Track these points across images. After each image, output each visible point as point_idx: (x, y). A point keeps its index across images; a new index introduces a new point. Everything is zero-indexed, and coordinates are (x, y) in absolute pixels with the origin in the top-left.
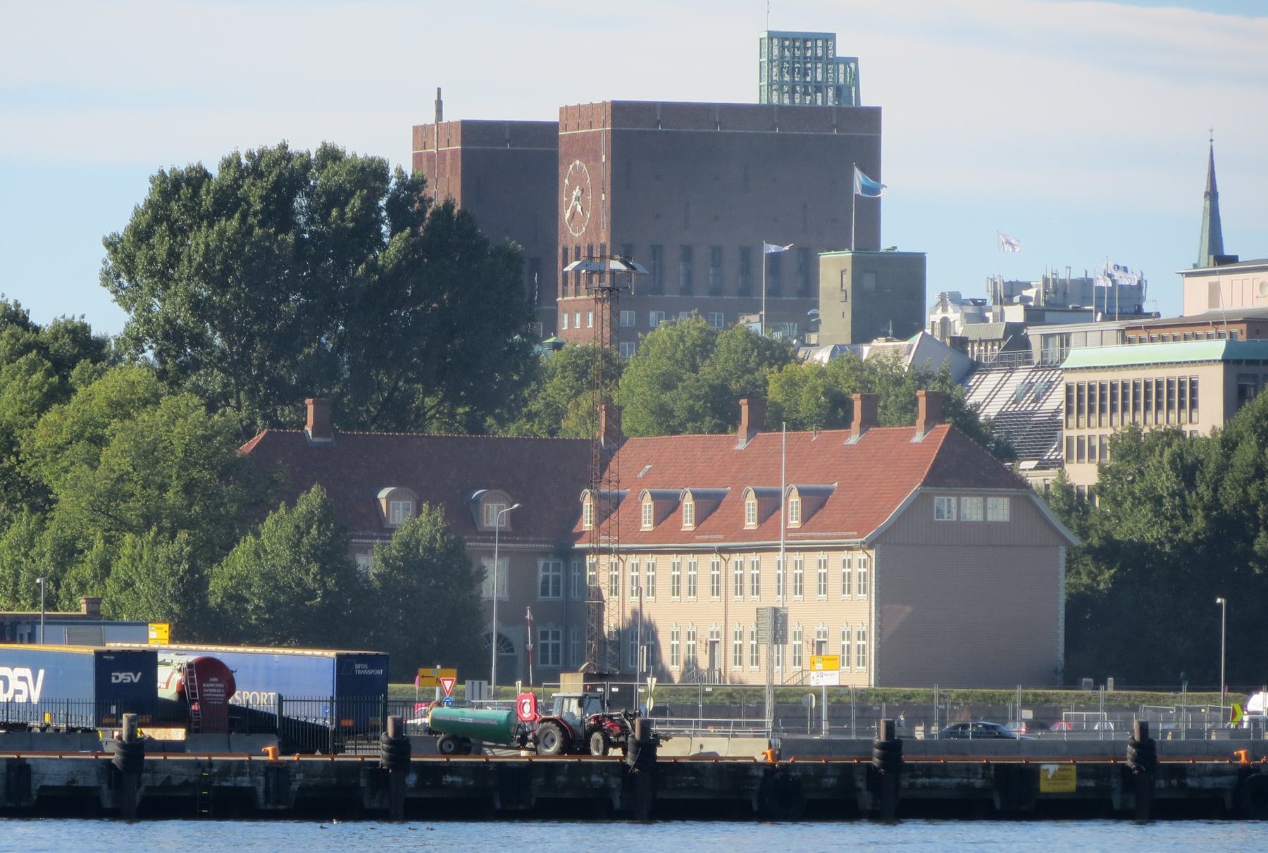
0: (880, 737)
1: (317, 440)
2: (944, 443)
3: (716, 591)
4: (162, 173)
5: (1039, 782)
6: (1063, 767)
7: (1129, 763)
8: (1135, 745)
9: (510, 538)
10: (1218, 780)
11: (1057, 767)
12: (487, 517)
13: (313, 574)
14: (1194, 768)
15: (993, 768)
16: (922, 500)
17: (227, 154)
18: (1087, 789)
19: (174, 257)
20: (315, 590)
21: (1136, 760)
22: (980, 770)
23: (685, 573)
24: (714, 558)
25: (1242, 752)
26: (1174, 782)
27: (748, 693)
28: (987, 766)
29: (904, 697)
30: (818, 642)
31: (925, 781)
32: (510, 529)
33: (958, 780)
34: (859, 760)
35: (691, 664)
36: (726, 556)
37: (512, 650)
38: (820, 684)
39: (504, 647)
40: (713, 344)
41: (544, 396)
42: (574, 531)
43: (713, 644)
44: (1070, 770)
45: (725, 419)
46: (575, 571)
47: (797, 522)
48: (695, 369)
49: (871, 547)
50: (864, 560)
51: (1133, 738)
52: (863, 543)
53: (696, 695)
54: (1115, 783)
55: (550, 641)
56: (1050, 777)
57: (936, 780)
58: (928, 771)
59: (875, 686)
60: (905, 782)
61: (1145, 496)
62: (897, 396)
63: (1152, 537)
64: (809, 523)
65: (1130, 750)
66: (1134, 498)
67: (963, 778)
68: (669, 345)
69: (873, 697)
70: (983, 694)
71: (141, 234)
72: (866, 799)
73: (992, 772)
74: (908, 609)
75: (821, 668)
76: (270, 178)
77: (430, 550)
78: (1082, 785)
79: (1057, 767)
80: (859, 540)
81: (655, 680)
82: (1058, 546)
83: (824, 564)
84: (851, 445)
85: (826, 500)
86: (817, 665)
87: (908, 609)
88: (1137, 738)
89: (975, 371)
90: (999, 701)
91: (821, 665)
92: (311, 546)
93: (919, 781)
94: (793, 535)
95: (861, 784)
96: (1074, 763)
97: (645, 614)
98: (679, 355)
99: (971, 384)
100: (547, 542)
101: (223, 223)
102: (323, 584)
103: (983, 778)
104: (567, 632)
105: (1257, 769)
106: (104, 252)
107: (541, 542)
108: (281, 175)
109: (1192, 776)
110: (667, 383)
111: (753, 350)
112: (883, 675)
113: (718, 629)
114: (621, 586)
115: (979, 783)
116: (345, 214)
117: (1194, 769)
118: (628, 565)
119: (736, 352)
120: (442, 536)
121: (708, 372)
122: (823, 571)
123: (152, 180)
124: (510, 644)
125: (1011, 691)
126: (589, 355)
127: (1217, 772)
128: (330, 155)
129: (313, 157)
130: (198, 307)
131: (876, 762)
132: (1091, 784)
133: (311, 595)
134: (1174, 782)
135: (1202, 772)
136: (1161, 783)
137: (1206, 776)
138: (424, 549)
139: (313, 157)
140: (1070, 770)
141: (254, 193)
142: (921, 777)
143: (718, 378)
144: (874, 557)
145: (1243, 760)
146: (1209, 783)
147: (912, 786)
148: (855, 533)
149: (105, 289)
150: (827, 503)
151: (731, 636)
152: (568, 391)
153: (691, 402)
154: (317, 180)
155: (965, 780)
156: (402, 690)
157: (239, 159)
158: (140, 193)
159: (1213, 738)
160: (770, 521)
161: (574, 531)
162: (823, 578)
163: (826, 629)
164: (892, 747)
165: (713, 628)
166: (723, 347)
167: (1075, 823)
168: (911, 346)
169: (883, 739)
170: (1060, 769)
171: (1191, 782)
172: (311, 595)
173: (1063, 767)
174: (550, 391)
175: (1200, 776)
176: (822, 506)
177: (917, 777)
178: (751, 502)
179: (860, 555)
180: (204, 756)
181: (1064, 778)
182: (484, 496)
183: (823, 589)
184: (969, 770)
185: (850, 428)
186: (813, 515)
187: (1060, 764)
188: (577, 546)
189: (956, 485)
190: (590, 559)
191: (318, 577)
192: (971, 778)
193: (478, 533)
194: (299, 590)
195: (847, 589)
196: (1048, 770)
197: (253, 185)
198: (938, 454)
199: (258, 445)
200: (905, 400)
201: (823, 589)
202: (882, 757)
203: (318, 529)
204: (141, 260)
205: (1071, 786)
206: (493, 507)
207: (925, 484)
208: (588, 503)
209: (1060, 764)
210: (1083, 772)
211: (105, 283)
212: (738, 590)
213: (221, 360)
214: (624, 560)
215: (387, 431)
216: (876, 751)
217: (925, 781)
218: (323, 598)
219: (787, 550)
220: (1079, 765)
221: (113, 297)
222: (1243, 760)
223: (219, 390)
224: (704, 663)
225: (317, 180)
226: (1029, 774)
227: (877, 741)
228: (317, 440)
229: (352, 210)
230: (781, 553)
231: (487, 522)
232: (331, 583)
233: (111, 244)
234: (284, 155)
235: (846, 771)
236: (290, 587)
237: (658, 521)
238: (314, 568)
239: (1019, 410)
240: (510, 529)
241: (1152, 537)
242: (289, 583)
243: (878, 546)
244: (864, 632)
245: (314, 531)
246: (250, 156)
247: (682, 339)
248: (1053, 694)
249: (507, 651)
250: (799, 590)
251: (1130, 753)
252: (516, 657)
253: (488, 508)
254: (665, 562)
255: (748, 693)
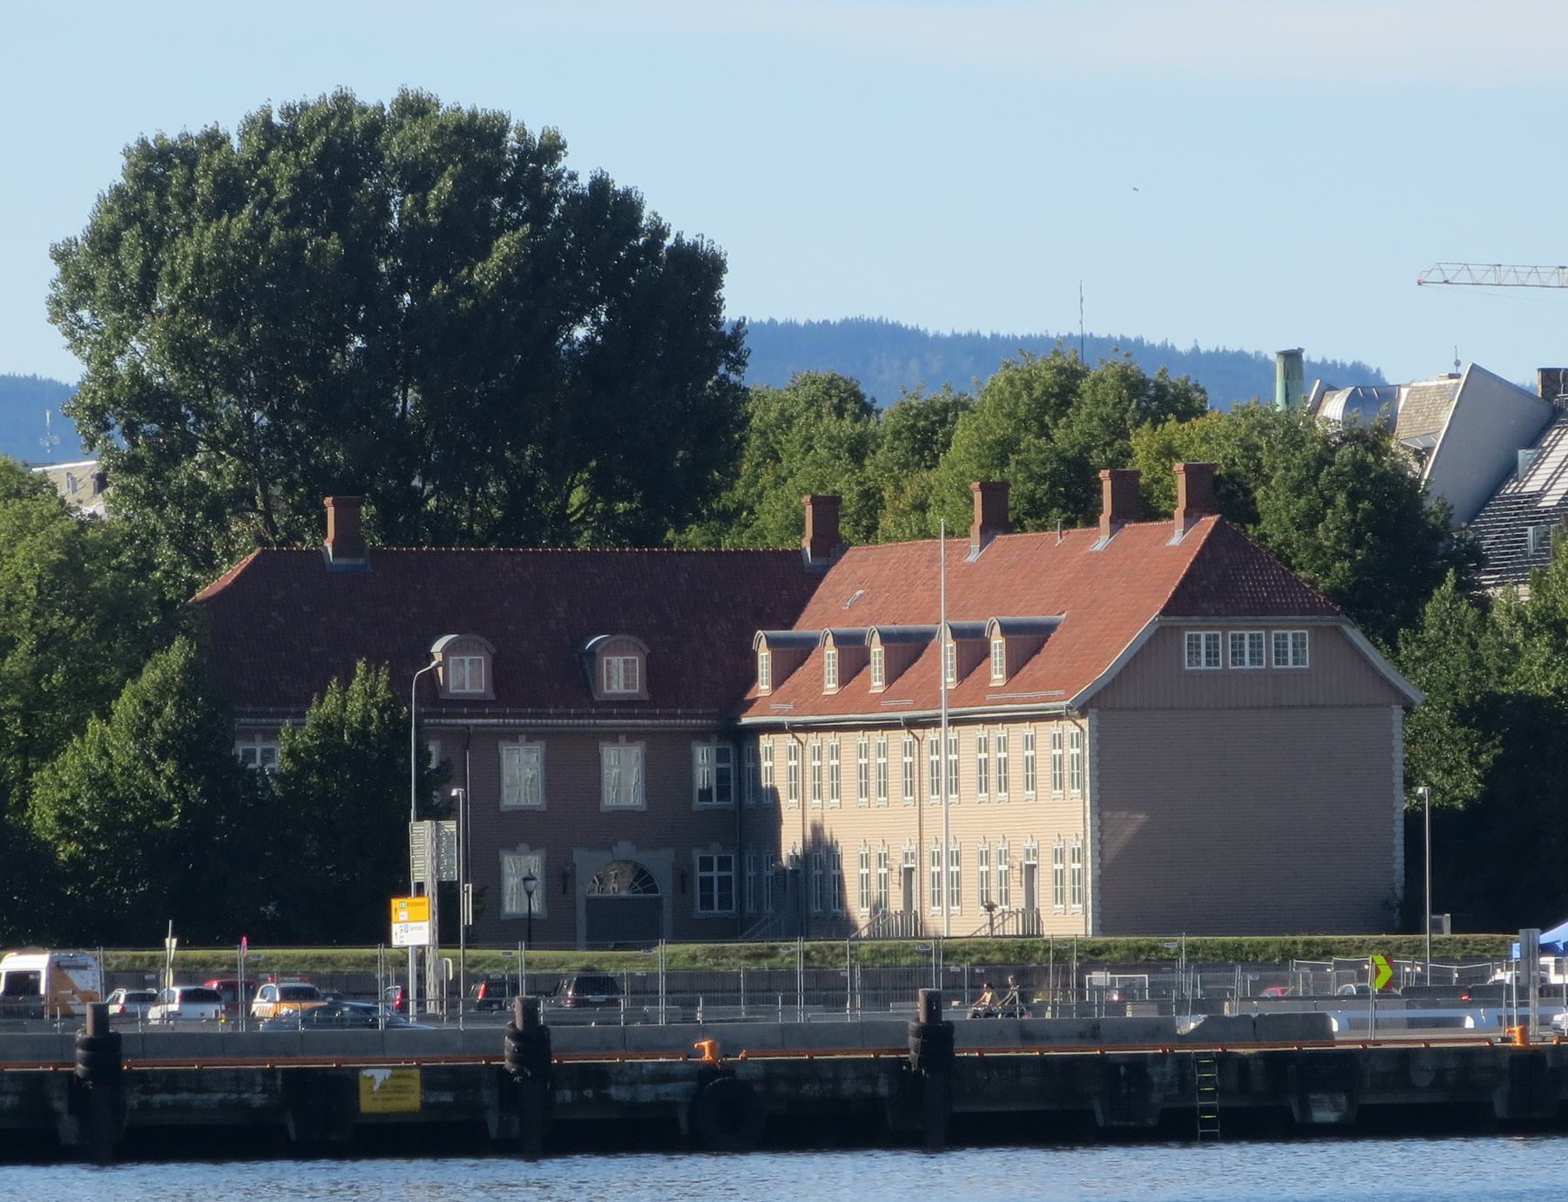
0: (87, 1030)
1: (343, 561)
2: (1204, 547)
3: (909, 789)
4: (144, 144)
5: (358, 1099)
6: (398, 1072)
7: (507, 1063)
8: (517, 1036)
9: (473, 711)
10: (662, 1089)
11: (388, 1073)
12: (609, 678)
13: (166, 777)
14: (621, 1069)
15: (279, 1075)
16: (1160, 640)
17: (254, 110)
18: (438, 1105)
19: (149, 276)
20: (171, 803)
21: (516, 1060)
22: (259, 1079)
23: (995, 755)
24: (903, 736)
25: (705, 1044)
26: (589, 1093)
27: (836, 951)
28: (272, 1073)
29: (1092, 951)
30: (1027, 866)
31: (168, 1098)
32: (646, 697)
33: (220, 1096)
34: (56, 1066)
35: (878, 907)
36: (801, 736)
37: (654, 889)
38: (405, 944)
39: (641, 884)
40: (1073, 391)
41: (862, 480)
42: (747, 698)
43: (908, 872)
44: (409, 1077)
45: (1082, 511)
46: (766, 760)
47: (1001, 676)
48: (1044, 431)
49: (1083, 715)
50: (1077, 734)
51: (513, 1025)
52: (1069, 707)
53: (929, 954)
54: (488, 1096)
55: (715, 873)
56: (376, 1088)
57: (185, 1096)
58: (172, 1082)
59: (1093, 935)
60: (133, 1101)
61: (1541, 622)
62: (1287, 469)
63: (1548, 686)
64: (1017, 677)
65: (509, 1043)
66: (1525, 623)
67: (231, 1092)
68: (1007, 394)
69: (1040, 953)
70: (1224, 945)
71: (104, 242)
72: (68, 1128)
73: (279, 1082)
74: (1142, 817)
75: (406, 918)
76: (312, 149)
77: (361, 735)
78: (432, 1100)
79: (388, 1073)
80: (1065, 703)
81: (174, 941)
82: (1389, 706)
83: (1030, 742)
84: (1098, 552)
85: (1046, 641)
86: (400, 913)
87: (1142, 817)
88: (519, 1025)
89: (1554, 422)
90: (1248, 953)
91: (405, 913)
92: (165, 732)
93: (157, 1098)
94: (996, 697)
95: (59, 1105)
96: (418, 1067)
97: (827, 833)
98: (1022, 411)
99: (1545, 444)
100: (707, 716)
101: (225, 220)
102: (183, 796)
103: (263, 1092)
104: (740, 856)
105: (729, 1070)
106: (54, 270)
107: (697, 716)
108: (328, 145)
109: (618, 1084)
110: (1003, 450)
111: (1131, 401)
112: (1106, 919)
113: (913, 848)
114: (917, 779)
115: (257, 1100)
116: (426, 202)
117: (621, 1072)
118: (926, 747)
119: (1105, 404)
120: (381, 712)
121: (1065, 436)
122: (1030, 753)
123: (127, 153)
124: (650, 879)
125: (367, 952)
126: (936, 413)
127: (662, 1076)
128: (414, 107)
129: (388, 110)
130: (183, 351)
131: (80, 1068)
132: (447, 1098)
133: (166, 810)
134: (589, 1093)
135: (637, 1077)
136: (567, 1095)
137: (643, 1083)
138: (352, 736)
139: (388, 110)
140: (409, 1077)
141: (283, 173)
142: (160, 1091)
143: (1073, 447)
144: (1087, 729)
145: (707, 1057)
146: (647, 1093)
147: (145, 1106)
148: (1061, 692)
149: (55, 327)
150: (1046, 645)
151: (927, 859)
152: (897, 472)
153: (1031, 486)
154: (394, 148)
155: (234, 1096)
156: (270, 958)
157: (269, 117)
158: (111, 173)
159: (1129, 1014)
160: (975, 676)
161: (747, 698)
162: (1030, 764)
163: (1035, 845)
164: (937, 1034)
165: (905, 849)
166: (1088, 398)
167: (29, 1167)
168: (1457, 384)
169: (90, 1033)
170: (392, 1076)
171: (616, 1093)
172: (166, 810)
173: (398, 1072)
174: (869, 470)
175: (632, 1083)
176: (1037, 650)
177: (153, 1091)
178: (830, 652)
179: (1069, 728)
180: (868, 1052)
181: (400, 1089)
182: (604, 643)
183: (1031, 783)
184: (240, 1080)
185: (1098, 526)
186: (1024, 664)
187: (393, 1068)
188: (745, 720)
189: (1218, 613)
190: (765, 741)
191: (176, 783)
192: (243, 1092)
193: (597, 705)
194: (146, 804)
195: (1058, 782)
196: (372, 1078)
197: (282, 159)
198: (1193, 563)
199: (244, 572)
200: (1300, 474)
201: (1031, 783)
202: (88, 1062)
203: (178, 705)
204: (102, 276)
205: (412, 1100)
206: (618, 661)
207: (1163, 613)
208: (764, 656)
209: (393, 1068)
210: (431, 1079)
211: (55, 318)
212: (818, 792)
213: (231, 437)
214: (803, 741)
215: (516, 546)
216: (79, 1051)
217: (168, 1098)
218: (183, 816)
219: (955, 722)
220: (425, 1070)
221: (67, 341)
222: (707, 1057)
223: (231, 486)
224: (896, 904)
225: (394, 148)
226: (344, 1085)
227: (79, 1035)
228: (343, 561)
229: (437, 198)
230: (943, 729)
231: (608, 688)
232: (194, 791)
233: (60, 256)
234: (343, 105)
235: (34, 1085)
236: (134, 799)
237: (844, 681)
238: (169, 768)
239: (1512, 492)
240: (646, 697)
241: (1548, 686)
242: (133, 793)
243: (1093, 712)
244: (1079, 849)
245: (169, 711)
246: (288, 112)
247: (1028, 386)
248: (1340, 942)
249: (645, 891)
250: (836, 792)
251: (508, 1050)
252: (660, 899)
253: (609, 663)
254: (969, 736)
255: (836, 951)
